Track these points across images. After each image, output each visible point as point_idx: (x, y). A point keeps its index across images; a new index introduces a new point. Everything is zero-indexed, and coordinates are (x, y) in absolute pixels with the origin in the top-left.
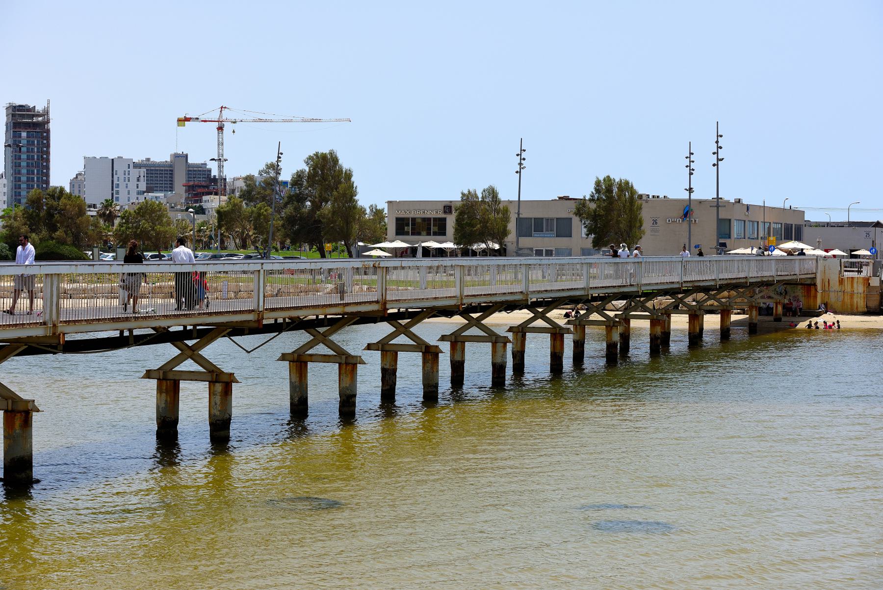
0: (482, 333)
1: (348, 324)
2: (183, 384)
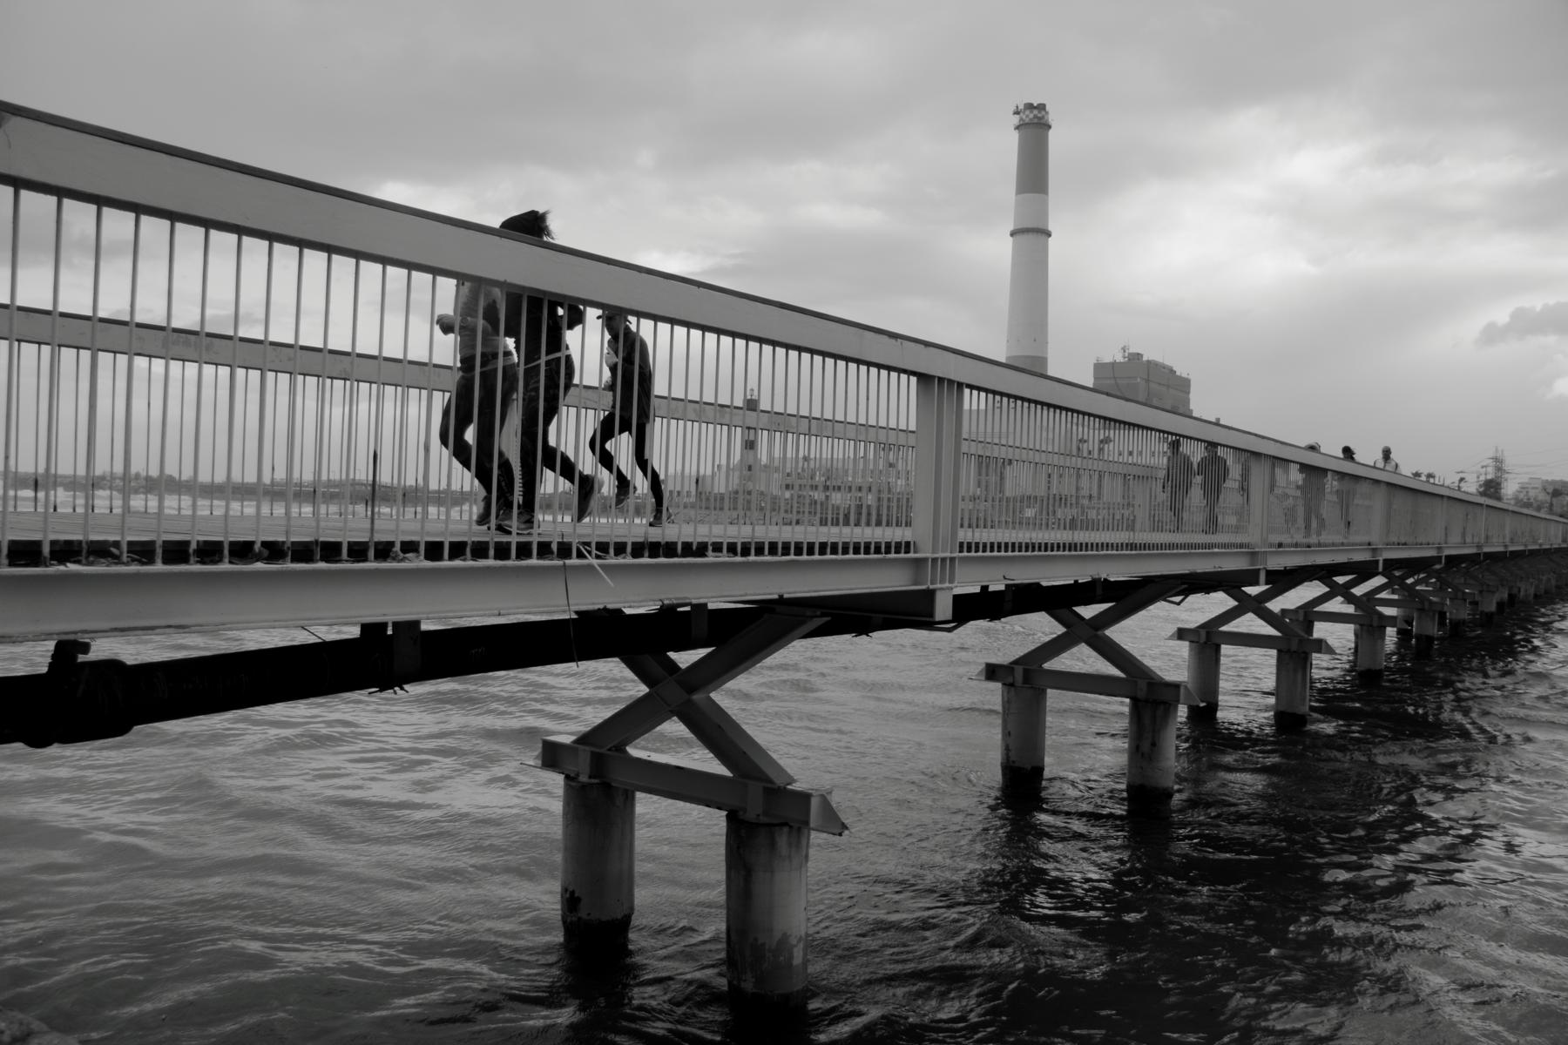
0: (703, 761)
1: (1174, 592)
2: (1226, 649)
